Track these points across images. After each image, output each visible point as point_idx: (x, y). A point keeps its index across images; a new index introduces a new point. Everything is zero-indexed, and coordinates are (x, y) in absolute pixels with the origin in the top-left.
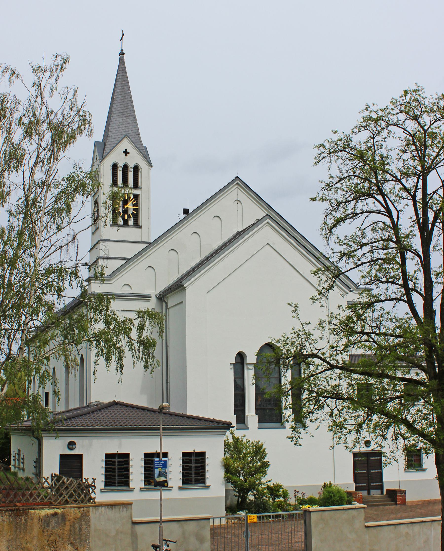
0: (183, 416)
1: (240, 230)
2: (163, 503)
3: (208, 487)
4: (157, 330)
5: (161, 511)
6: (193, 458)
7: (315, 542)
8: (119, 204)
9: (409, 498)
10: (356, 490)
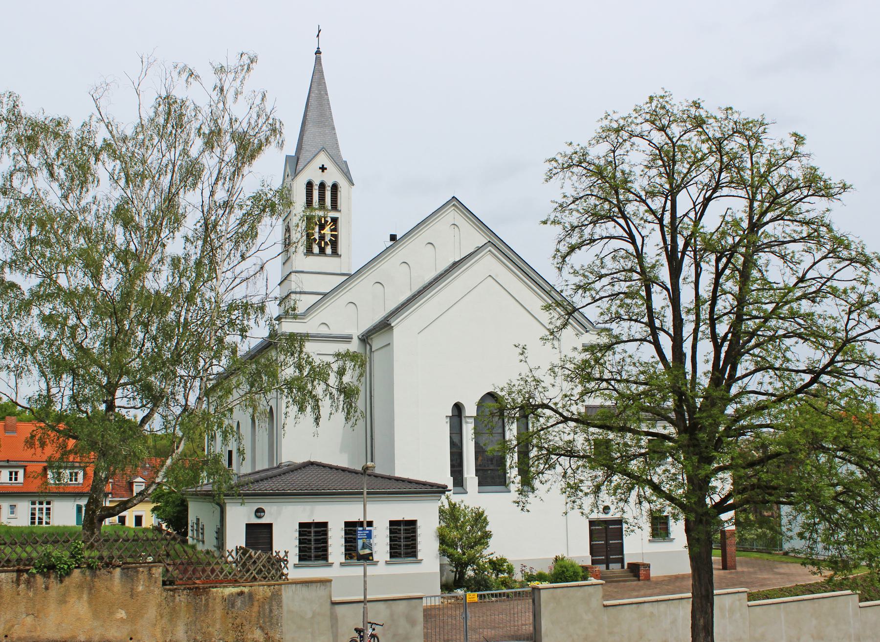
0: (390, 478)
4: (359, 376)
5: (365, 589)
6: (402, 528)
7: (545, 624)
8: (313, 229)
9: (653, 574)
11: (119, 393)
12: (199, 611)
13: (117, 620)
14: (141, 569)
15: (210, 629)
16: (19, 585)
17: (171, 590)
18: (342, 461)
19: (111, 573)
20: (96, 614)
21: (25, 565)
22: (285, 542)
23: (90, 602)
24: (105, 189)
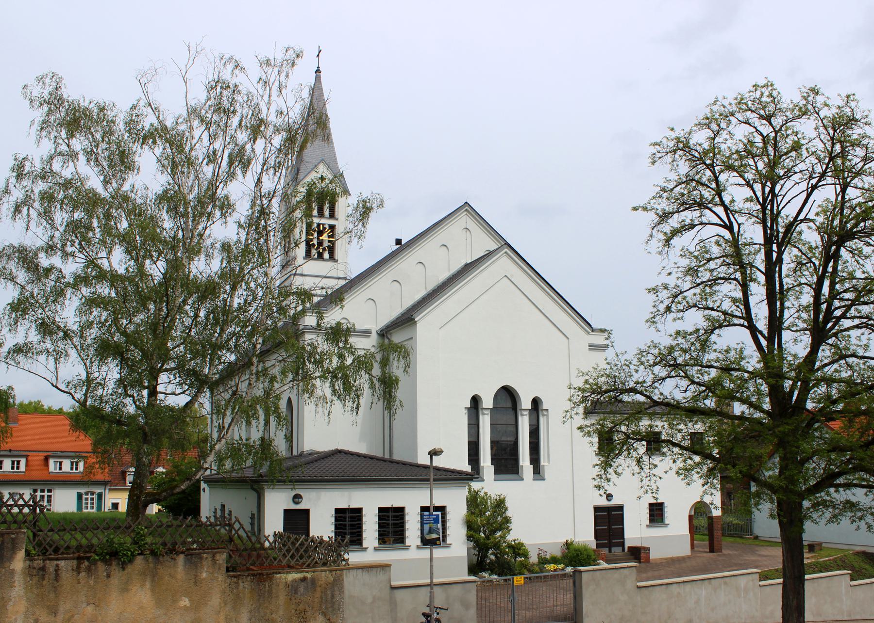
0: (412, 465)
1: (469, 262)
2: (434, 564)
3: (449, 546)
4: (385, 368)
5: (432, 574)
6: (390, 514)
7: (587, 605)
8: (312, 235)
9: (653, 555)
10: (597, 547)
11: (163, 378)
12: (263, 596)
13: (180, 608)
14: (205, 555)
15: (274, 615)
16: (79, 573)
17: (235, 577)
18: (361, 448)
19: (175, 559)
20: (159, 601)
21: (86, 552)
22: (322, 527)
23: (153, 590)
24: (148, 177)
